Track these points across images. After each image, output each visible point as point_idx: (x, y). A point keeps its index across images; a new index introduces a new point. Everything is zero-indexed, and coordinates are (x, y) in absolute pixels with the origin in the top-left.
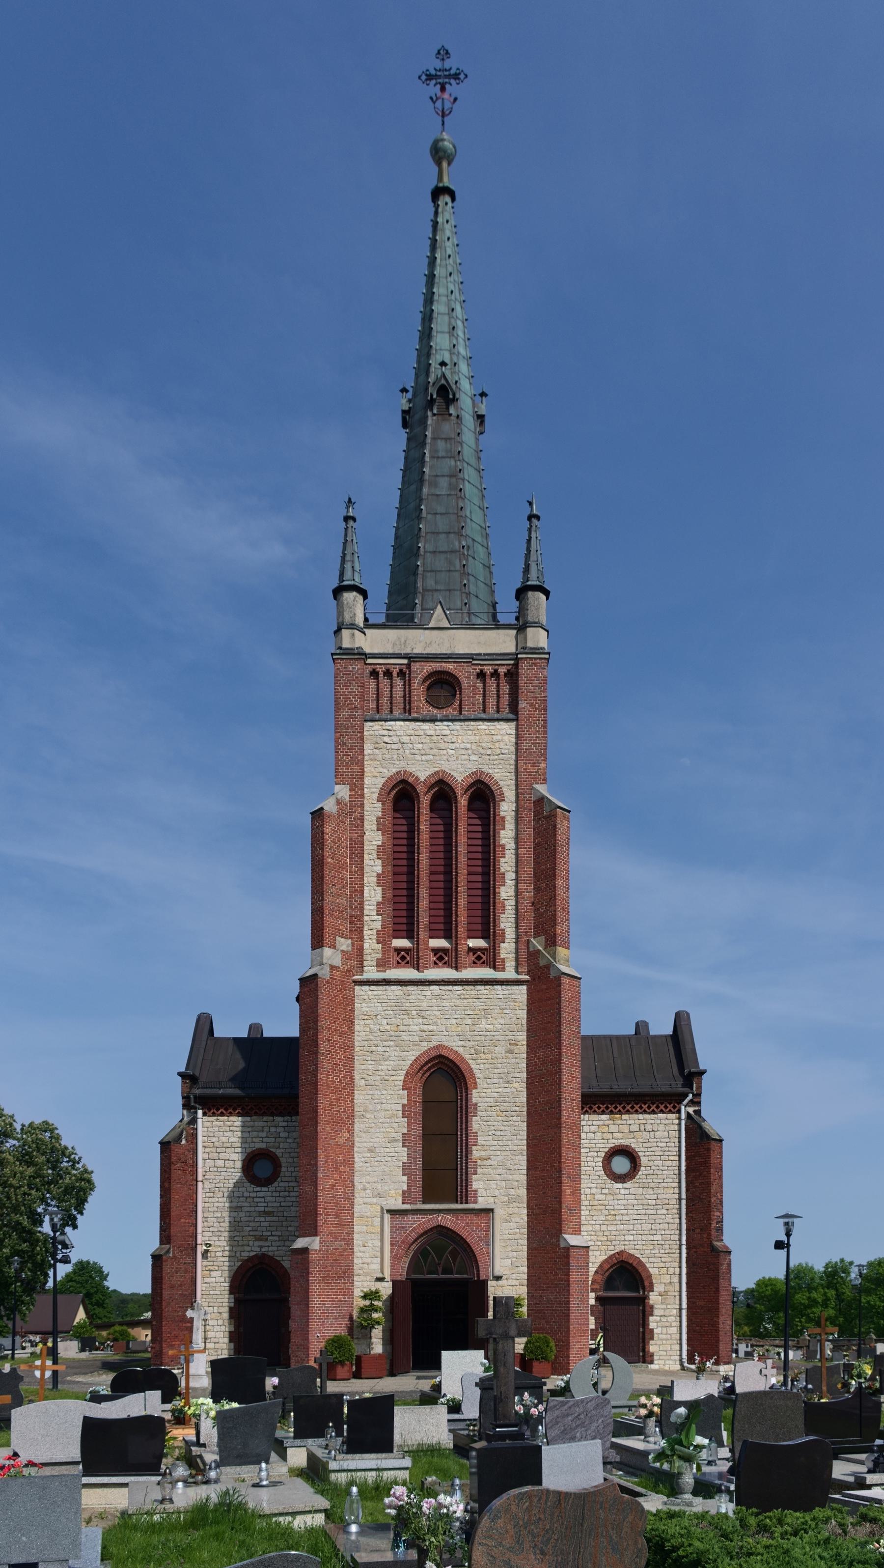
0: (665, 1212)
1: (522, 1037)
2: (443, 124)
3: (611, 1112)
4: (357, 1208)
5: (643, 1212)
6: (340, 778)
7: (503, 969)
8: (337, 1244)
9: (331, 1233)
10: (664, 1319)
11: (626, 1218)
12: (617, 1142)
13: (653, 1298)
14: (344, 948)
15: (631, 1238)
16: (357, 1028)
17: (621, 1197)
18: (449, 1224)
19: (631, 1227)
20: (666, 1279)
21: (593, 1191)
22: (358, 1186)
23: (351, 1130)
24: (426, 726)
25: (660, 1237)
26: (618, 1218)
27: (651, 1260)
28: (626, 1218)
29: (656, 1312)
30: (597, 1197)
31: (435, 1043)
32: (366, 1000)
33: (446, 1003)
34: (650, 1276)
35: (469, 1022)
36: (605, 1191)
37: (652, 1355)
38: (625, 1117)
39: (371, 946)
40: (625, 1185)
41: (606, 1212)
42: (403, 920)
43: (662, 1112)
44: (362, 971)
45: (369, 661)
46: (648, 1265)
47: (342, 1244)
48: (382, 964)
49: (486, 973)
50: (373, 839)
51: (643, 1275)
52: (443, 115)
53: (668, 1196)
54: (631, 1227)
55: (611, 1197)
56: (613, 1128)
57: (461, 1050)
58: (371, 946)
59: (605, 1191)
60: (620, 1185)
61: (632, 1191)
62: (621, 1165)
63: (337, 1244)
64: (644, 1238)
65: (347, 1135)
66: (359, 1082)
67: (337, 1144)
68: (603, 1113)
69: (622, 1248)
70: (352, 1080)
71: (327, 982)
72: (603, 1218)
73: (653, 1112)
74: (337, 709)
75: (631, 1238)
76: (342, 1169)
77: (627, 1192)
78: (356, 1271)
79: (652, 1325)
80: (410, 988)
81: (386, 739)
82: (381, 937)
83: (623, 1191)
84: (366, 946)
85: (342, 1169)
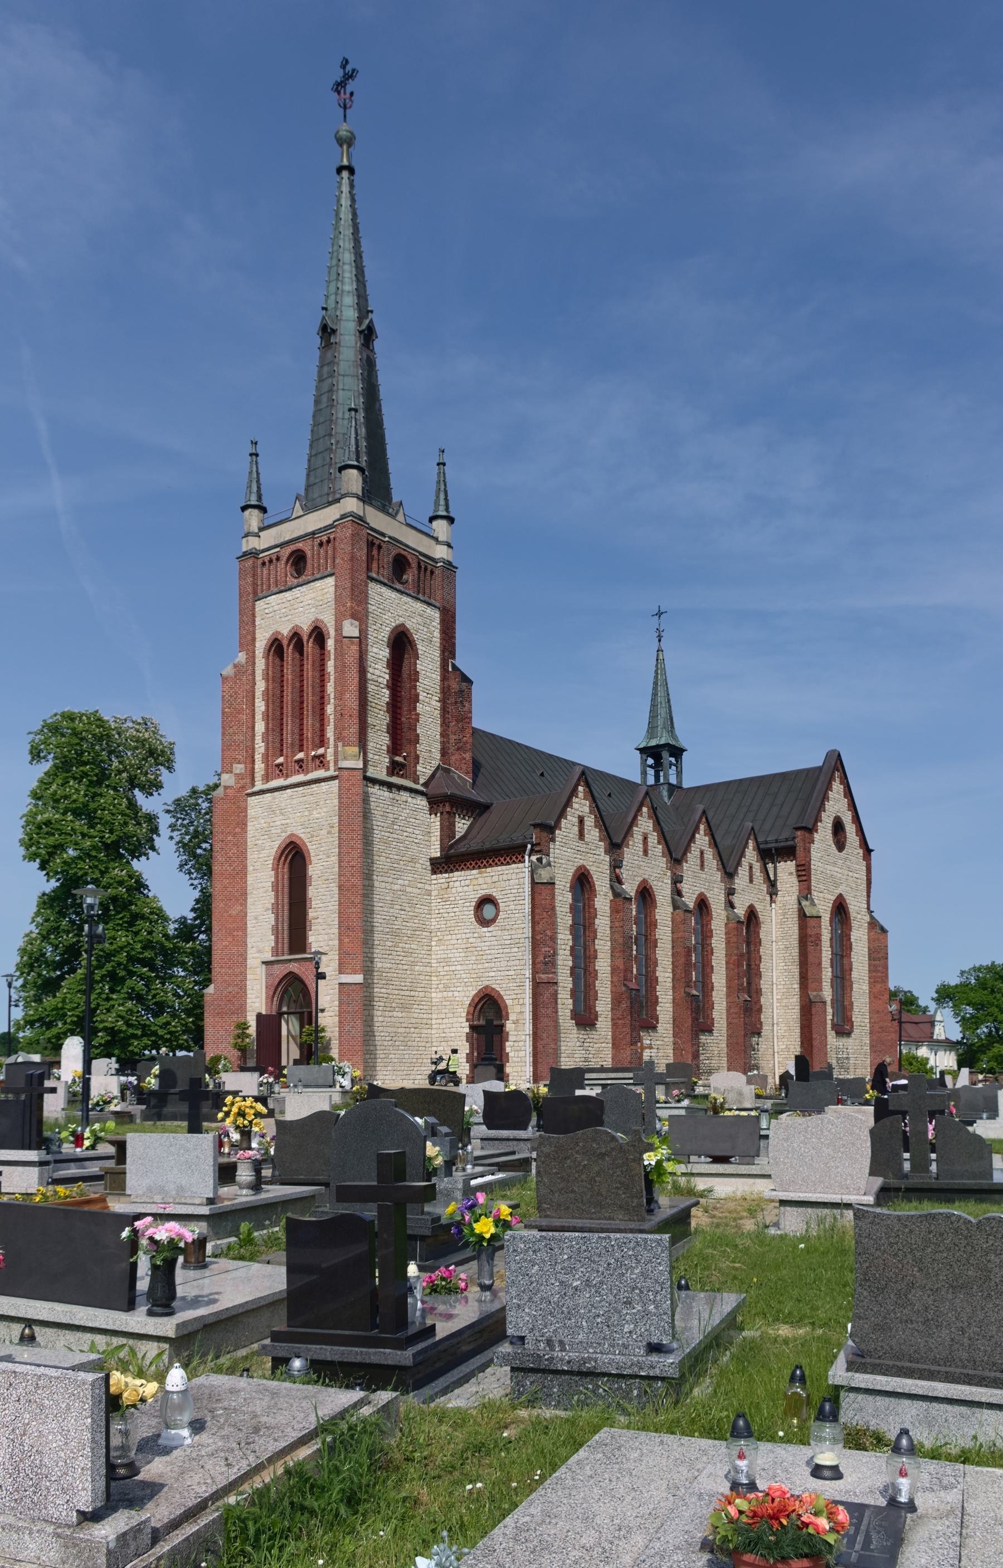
0: (516, 950)
1: (336, 820)
2: (345, 116)
3: (479, 867)
4: (249, 962)
5: (501, 951)
6: (242, 647)
7: (328, 769)
8: (230, 989)
9: (225, 981)
10: (516, 1044)
11: (490, 957)
12: (483, 892)
13: (509, 1026)
14: (238, 772)
15: (493, 974)
16: (249, 828)
17: (485, 939)
18: (296, 971)
19: (493, 965)
20: (518, 1009)
21: (468, 936)
22: (249, 945)
23: (244, 904)
24: (287, 594)
25: (513, 973)
26: (484, 957)
27: (507, 992)
28: (490, 957)
29: (511, 1038)
30: (471, 940)
31: (289, 833)
32: (255, 806)
33: (295, 801)
34: (506, 1006)
35: (307, 813)
36: (476, 935)
37: (508, 1076)
38: (489, 870)
39: (259, 766)
40: (490, 929)
41: (476, 953)
42: (277, 743)
43: (514, 862)
44: (253, 785)
45: (261, 555)
46: (505, 997)
47: (236, 989)
48: (267, 778)
49: (321, 773)
50: (261, 686)
51: (502, 1005)
52: (345, 108)
53: (519, 936)
54: (493, 965)
55: (479, 940)
56: (481, 881)
57: (302, 836)
58: (259, 766)
59: (476, 935)
60: (485, 929)
61: (494, 933)
62: (488, 911)
63: (230, 989)
64: (502, 973)
65: (239, 908)
66: (250, 868)
67: (230, 916)
68: (474, 868)
69: (487, 983)
70: (245, 867)
71: (222, 799)
72: (474, 958)
73: (508, 864)
74: (241, 597)
75: (493, 974)
76: (235, 933)
77: (490, 934)
78: (248, 1009)
79: (508, 1050)
80: (276, 794)
81: (267, 611)
82: (266, 757)
83: (488, 934)
84: (256, 766)
85: (235, 933)
